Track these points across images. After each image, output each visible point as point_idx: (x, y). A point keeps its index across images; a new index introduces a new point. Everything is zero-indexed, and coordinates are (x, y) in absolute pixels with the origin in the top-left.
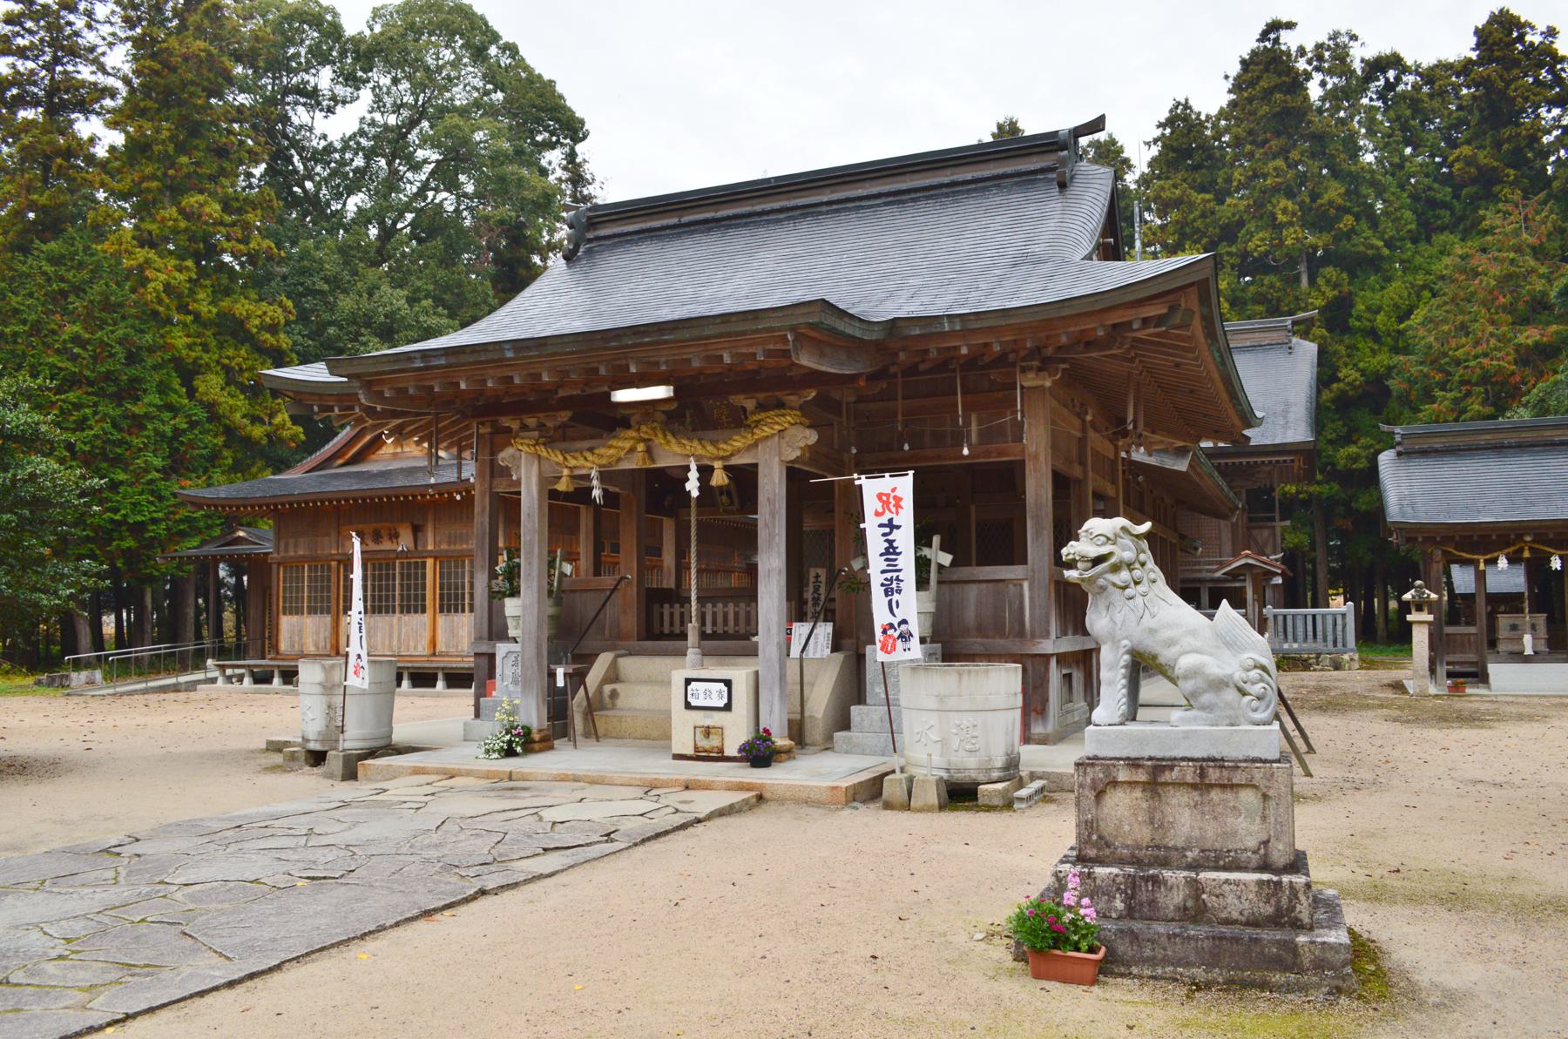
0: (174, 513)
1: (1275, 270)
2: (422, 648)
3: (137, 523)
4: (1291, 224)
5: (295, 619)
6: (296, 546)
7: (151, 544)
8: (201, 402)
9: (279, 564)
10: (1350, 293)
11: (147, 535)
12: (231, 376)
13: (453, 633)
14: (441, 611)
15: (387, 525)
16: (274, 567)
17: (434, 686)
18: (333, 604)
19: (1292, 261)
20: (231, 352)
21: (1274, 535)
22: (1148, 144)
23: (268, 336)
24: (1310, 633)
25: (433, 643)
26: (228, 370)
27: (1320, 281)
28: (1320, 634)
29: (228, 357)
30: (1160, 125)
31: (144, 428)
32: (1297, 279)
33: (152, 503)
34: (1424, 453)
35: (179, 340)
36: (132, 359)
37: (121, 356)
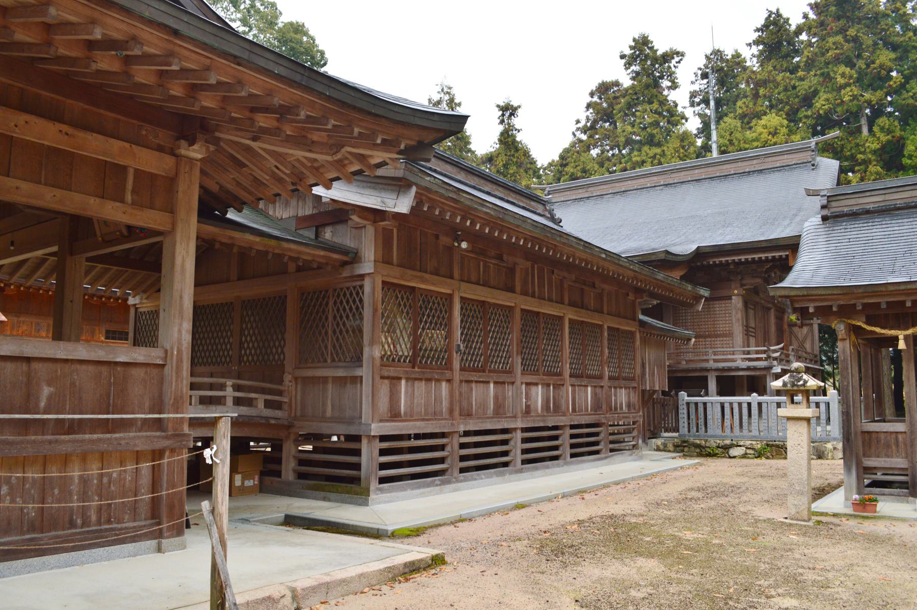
1: (837, 124)
4: (847, 85)
10: (902, 138)
19: (855, 115)
21: (812, 331)
22: (749, 45)
27: (875, 129)
30: (757, 30)
32: (859, 130)
34: (854, 215)
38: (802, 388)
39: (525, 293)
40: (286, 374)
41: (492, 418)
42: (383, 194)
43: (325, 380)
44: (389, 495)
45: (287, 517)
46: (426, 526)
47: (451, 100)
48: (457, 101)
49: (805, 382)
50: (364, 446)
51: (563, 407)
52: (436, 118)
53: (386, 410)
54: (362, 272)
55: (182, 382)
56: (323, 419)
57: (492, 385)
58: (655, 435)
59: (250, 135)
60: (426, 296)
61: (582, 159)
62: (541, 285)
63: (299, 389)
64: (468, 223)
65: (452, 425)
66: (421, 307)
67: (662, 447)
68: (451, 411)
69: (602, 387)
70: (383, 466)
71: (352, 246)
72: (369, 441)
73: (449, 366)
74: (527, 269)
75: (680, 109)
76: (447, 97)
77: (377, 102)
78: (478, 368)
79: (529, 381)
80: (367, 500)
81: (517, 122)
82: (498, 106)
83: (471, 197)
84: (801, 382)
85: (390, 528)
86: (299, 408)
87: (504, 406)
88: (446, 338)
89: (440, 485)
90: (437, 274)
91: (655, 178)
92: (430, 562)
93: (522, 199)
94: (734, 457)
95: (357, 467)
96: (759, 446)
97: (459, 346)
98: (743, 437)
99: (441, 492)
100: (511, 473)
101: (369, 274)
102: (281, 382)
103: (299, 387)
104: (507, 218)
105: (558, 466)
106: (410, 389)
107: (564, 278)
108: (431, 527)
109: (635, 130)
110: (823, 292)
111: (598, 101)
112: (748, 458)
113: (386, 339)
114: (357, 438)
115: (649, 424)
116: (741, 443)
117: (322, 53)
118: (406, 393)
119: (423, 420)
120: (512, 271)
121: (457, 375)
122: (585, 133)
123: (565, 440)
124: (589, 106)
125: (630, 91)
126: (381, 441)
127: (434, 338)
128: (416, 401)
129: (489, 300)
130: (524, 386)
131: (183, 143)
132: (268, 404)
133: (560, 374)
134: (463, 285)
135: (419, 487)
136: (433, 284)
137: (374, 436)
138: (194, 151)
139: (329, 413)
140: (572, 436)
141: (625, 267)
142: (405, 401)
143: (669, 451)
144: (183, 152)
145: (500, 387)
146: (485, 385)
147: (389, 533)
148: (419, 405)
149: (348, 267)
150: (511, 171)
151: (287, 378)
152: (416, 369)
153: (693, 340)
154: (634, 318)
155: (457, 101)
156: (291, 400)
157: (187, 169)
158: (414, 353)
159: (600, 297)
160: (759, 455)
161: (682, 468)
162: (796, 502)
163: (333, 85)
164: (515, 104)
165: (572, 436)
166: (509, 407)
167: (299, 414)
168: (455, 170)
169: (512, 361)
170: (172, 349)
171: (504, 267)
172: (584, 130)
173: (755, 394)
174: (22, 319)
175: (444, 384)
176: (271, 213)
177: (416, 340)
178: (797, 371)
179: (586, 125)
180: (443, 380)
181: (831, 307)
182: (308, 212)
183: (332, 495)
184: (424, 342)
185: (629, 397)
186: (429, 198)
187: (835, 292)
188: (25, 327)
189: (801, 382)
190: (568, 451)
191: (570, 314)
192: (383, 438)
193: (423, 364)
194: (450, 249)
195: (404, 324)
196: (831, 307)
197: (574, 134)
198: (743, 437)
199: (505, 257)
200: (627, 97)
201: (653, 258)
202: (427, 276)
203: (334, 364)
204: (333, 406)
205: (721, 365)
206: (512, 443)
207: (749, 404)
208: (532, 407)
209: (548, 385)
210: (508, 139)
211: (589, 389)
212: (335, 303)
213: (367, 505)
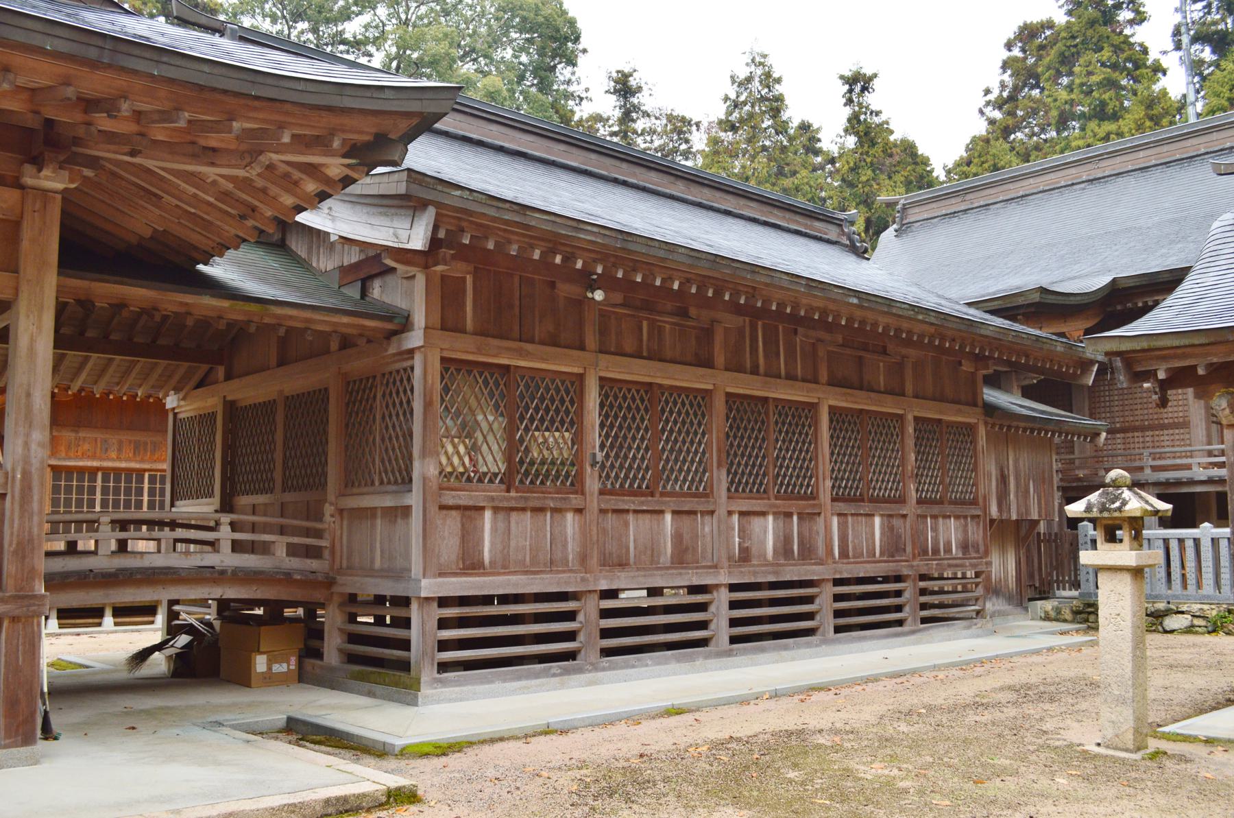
38: (1116, 514)
39: (735, 367)
40: (327, 505)
41: (667, 568)
42: (396, 224)
43: (371, 512)
44: (457, 689)
45: (290, 720)
46: (474, 739)
47: (768, 75)
48: (776, 75)
49: (1124, 503)
50: (415, 613)
51: (821, 551)
52: (388, 94)
53: (454, 557)
54: (410, 346)
55: (31, 519)
56: (371, 572)
57: (668, 517)
58: (1043, 595)
59: (127, 149)
60: (533, 379)
61: (993, 151)
62: (771, 354)
63: (345, 527)
64: (558, 259)
65: (583, 579)
66: (522, 397)
67: (1053, 614)
68: (583, 558)
69: (904, 516)
70: (444, 645)
71: (404, 307)
72: (421, 606)
73: (578, 485)
74: (741, 331)
75: (1153, 55)
76: (759, 71)
77: (260, 79)
78: (634, 488)
79: (744, 509)
80: (416, 697)
81: (872, 100)
82: (842, 77)
83: (552, 218)
84: (1117, 504)
85: (399, 743)
86: (345, 557)
87: (695, 550)
88: (573, 444)
89: (561, 675)
90: (555, 344)
91: (1073, 171)
92: (384, 799)
93: (798, 218)
94: (1172, 632)
95: (405, 645)
96: (1214, 613)
97: (594, 455)
98: (1188, 598)
99: (562, 686)
100: (707, 657)
101: (419, 348)
102: (319, 517)
103: (345, 523)
104: (631, 247)
105: (809, 645)
106: (501, 525)
107: (819, 340)
108: (483, 742)
109: (1073, 96)
110: (1176, 343)
111: (1020, 55)
112: (1196, 633)
113: (455, 447)
114: (405, 602)
115: (1031, 576)
116: (1184, 608)
117: (572, 23)
118: (494, 530)
119: (526, 573)
120: (707, 334)
121: (593, 502)
122: (1000, 108)
123: (824, 603)
124: (1005, 66)
125: (1063, 34)
126: (440, 606)
127: (551, 444)
128: (513, 544)
129: (659, 381)
130: (736, 517)
131: (28, 169)
132: (293, 551)
133: (814, 496)
134: (604, 359)
135: (519, 678)
136: (543, 360)
137: (427, 599)
138: (47, 178)
139: (378, 564)
140: (838, 598)
141: (910, 319)
142: (492, 544)
143: (1065, 621)
144: (28, 181)
145: (686, 521)
146: (655, 516)
147: (397, 750)
148: (517, 551)
149: (395, 339)
150: (864, 179)
151: (328, 509)
152: (513, 494)
153: (1104, 435)
154: (974, 401)
155: (776, 75)
156: (333, 545)
157: (37, 206)
158: (509, 468)
159: (899, 368)
160: (1214, 628)
161: (1050, 649)
162: (1113, 717)
163: (165, 59)
164: (868, 71)
165: (838, 598)
166: (704, 550)
167: (344, 565)
168: (666, 179)
169: (711, 477)
170: (13, 470)
171: (694, 328)
172: (999, 104)
173: (1206, 524)
174: (82, 434)
175: (570, 516)
176: (314, 265)
177: (513, 448)
178: (1116, 484)
179: (1001, 95)
180: (567, 510)
181: (1194, 367)
182: (354, 259)
183: (379, 689)
184: (527, 450)
185: (965, 531)
186: (471, 222)
187: (1196, 342)
188: (86, 446)
189: (1117, 504)
190: (829, 622)
191: (830, 399)
192: (443, 602)
193: (528, 482)
194: (581, 303)
195: (490, 426)
196: (1194, 367)
197: (981, 112)
198: (1188, 598)
199: (693, 312)
200: (1059, 45)
201: (1021, 301)
202: (529, 347)
203: (384, 488)
204: (382, 551)
205: (1163, 476)
206: (712, 608)
207: (1197, 541)
208: (754, 551)
209: (789, 515)
210: (864, 128)
211: (877, 520)
212: (384, 395)
213: (416, 705)
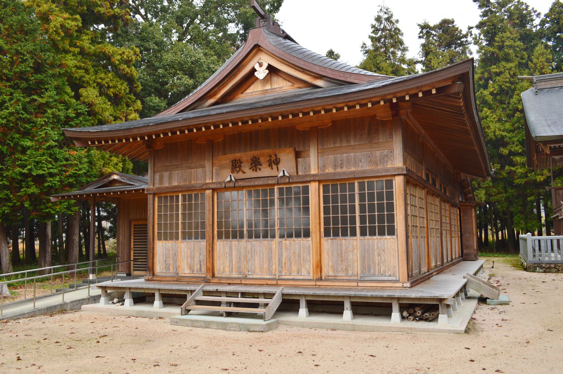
0: (65, 171)
2: (307, 272)
3: (38, 176)
5: (169, 244)
6: (170, 178)
7: (50, 190)
8: (84, 103)
9: (154, 194)
11: (46, 185)
12: (102, 90)
13: (341, 256)
14: (327, 234)
15: (267, 151)
16: (150, 197)
17: (341, 313)
18: (208, 229)
20: (103, 75)
23: (125, 66)
24: (549, 248)
25: (319, 266)
26: (100, 86)
28: (542, 248)
29: (101, 78)
31: (46, 112)
33: (50, 162)
35: (70, 61)
36: (38, 68)
37: (31, 63)
